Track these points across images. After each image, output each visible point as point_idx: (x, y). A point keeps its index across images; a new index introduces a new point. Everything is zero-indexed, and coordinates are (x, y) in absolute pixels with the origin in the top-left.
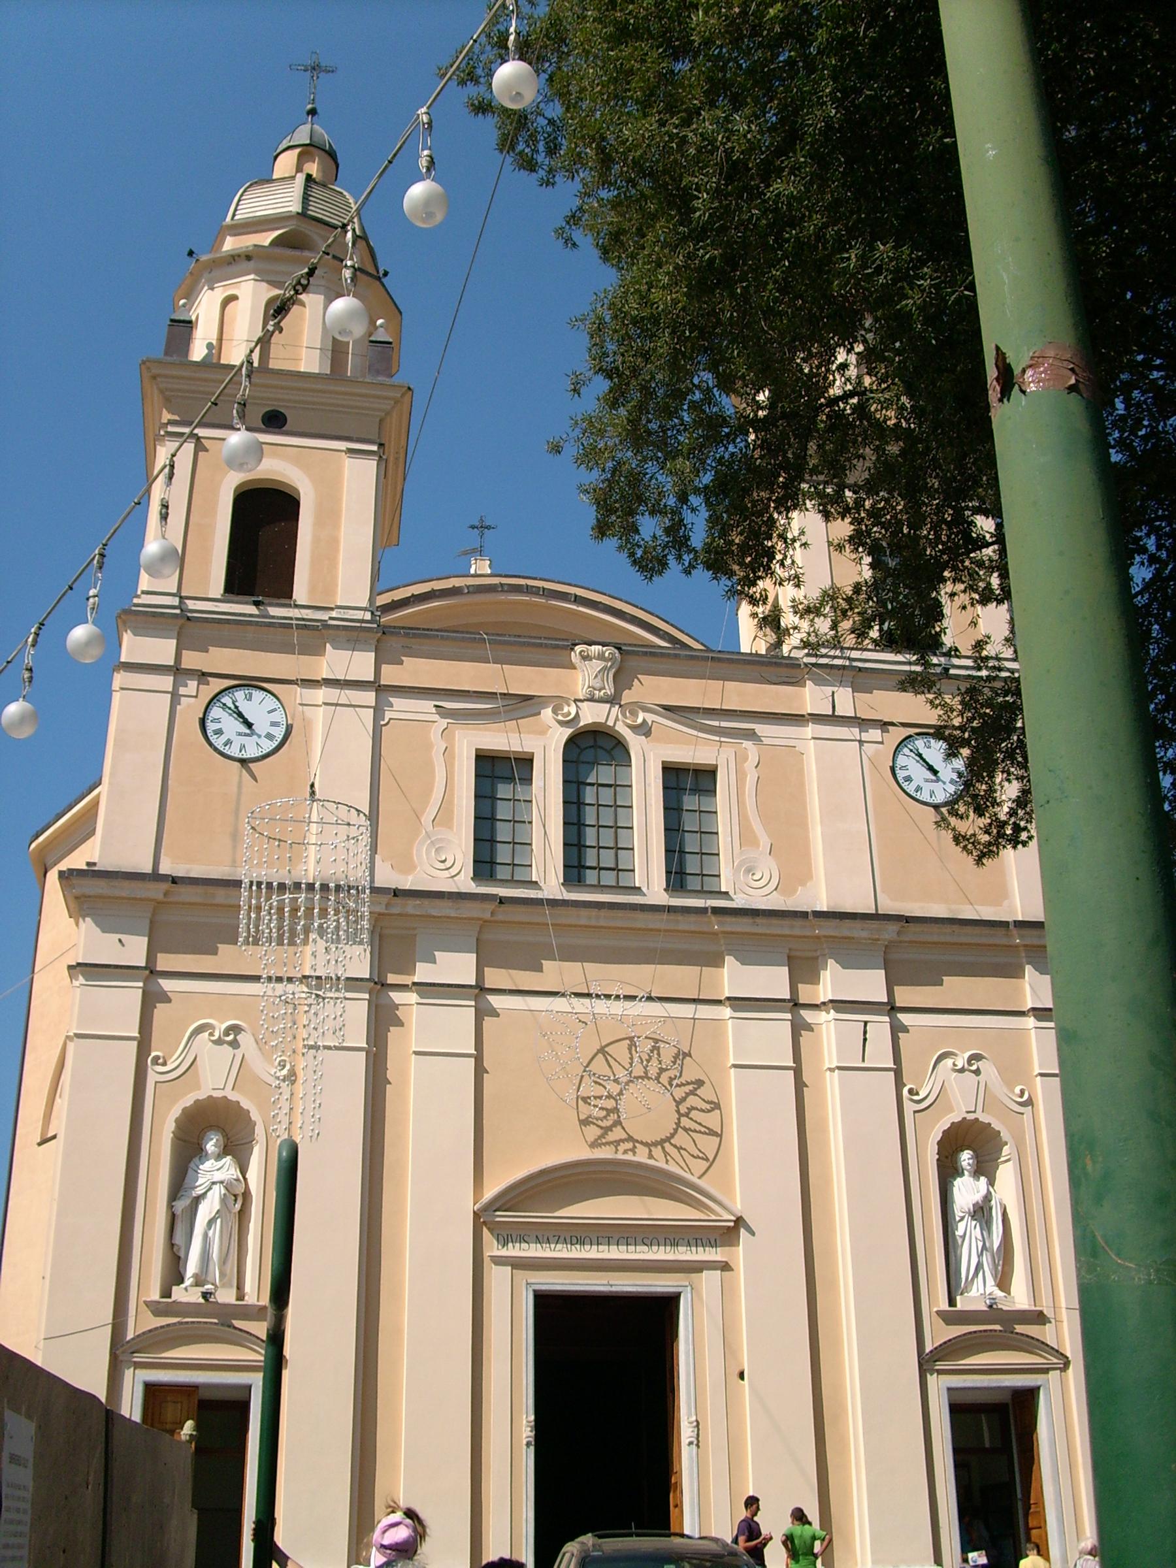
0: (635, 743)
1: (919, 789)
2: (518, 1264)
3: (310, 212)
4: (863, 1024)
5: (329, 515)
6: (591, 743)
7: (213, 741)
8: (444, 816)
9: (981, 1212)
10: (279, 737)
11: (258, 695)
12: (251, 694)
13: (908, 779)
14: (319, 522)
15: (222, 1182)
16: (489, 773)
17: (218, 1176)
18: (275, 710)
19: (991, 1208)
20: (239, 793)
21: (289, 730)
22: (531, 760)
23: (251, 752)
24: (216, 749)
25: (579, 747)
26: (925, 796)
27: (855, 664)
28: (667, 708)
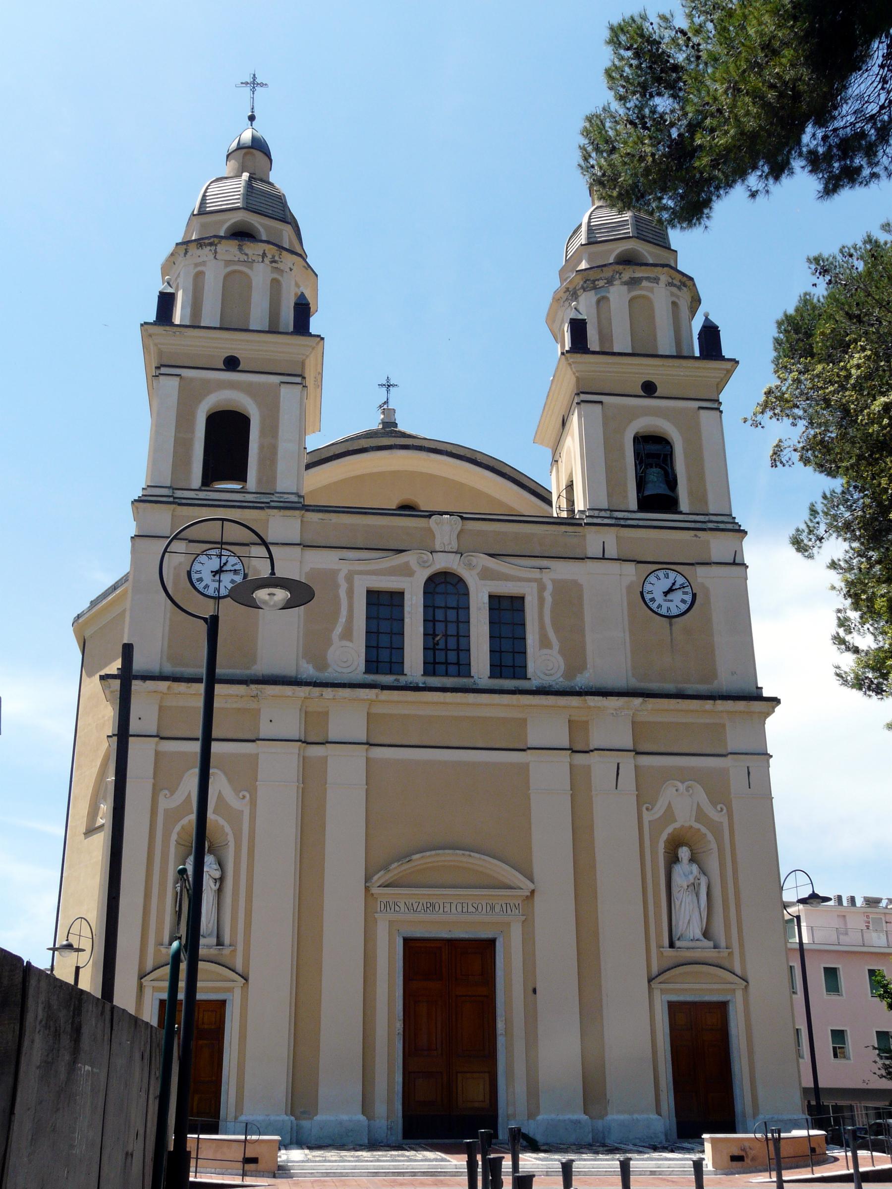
1: (659, 606)
3: (208, 209)
6: (443, 580)
7: (197, 586)
8: (347, 634)
14: (263, 433)
21: (694, 596)
23: (675, 611)
25: (435, 583)
26: (663, 611)
27: (177, 500)
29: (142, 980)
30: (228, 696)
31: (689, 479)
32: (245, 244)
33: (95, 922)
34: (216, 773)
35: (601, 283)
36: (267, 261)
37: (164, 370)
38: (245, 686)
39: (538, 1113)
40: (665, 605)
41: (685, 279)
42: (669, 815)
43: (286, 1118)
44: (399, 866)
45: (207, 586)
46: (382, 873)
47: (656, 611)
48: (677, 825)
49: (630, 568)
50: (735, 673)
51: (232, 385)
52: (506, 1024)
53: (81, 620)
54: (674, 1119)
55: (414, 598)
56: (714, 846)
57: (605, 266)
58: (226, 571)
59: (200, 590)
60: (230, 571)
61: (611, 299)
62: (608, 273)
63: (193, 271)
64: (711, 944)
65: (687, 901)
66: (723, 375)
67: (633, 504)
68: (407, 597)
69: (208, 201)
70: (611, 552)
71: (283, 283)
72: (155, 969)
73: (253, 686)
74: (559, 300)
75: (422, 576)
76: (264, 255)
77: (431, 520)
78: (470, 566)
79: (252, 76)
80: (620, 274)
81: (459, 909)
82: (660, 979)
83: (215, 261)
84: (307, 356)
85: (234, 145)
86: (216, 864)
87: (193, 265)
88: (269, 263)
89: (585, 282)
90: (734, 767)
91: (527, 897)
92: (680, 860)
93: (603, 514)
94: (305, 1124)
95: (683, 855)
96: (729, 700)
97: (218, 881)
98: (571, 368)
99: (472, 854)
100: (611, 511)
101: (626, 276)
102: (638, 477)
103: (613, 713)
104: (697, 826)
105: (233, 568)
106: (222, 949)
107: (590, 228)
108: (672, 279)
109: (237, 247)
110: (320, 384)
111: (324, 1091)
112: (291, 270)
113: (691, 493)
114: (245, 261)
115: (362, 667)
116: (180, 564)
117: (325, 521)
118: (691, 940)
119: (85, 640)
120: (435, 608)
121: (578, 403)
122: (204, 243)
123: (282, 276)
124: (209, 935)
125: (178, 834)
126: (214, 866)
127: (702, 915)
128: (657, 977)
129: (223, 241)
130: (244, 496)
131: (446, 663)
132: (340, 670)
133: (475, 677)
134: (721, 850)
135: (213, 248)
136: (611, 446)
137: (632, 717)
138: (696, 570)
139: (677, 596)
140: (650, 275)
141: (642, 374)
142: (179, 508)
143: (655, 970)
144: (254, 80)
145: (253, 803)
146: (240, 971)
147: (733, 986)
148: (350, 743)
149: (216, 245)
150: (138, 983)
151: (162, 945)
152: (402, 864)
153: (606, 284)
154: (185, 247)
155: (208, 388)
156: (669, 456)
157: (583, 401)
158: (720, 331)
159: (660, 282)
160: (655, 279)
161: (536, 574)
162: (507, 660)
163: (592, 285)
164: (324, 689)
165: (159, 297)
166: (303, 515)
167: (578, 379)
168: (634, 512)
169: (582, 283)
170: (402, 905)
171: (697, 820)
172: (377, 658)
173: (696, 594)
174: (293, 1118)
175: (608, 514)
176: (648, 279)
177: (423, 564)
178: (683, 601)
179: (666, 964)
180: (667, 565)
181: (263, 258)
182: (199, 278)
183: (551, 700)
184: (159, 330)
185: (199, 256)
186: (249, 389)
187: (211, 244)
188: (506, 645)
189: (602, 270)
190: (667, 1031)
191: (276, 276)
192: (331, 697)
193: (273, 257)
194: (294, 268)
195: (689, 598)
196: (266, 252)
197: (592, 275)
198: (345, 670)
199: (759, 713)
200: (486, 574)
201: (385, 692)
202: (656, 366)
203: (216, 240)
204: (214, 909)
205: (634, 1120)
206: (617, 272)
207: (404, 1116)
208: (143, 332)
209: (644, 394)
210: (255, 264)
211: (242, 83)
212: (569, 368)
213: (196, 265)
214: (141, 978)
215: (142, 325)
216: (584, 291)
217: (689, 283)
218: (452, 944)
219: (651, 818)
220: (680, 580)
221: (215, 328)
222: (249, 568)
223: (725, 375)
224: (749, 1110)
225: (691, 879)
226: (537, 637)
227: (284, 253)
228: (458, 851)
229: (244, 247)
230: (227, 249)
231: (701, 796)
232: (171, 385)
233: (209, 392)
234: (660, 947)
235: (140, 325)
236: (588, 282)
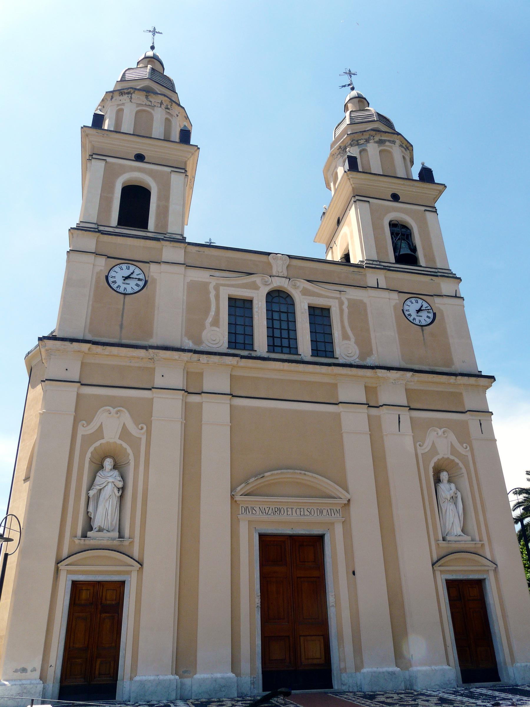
1: (414, 319)
7: (112, 286)
8: (216, 323)
9: (454, 499)
12: (129, 267)
14: (159, 199)
20: (123, 309)
21: (435, 314)
24: (113, 289)
26: (417, 322)
29: (58, 565)
30: (132, 357)
31: (424, 249)
32: (150, 95)
33: (23, 516)
34: (122, 410)
35: (362, 142)
36: (163, 107)
37: (94, 156)
38: (145, 350)
39: (362, 667)
40: (418, 319)
41: (409, 145)
42: (434, 450)
43: (172, 677)
44: (255, 480)
45: (119, 287)
46: (243, 485)
47: (413, 322)
48: (439, 457)
49: (395, 295)
50: (465, 361)
51: (140, 170)
52: (335, 598)
53: (30, 355)
54: (459, 668)
55: (260, 303)
56: (464, 470)
57: (365, 131)
58: (133, 278)
59: (114, 288)
60: (136, 278)
61: (369, 150)
62: (366, 136)
63: (115, 109)
64: (469, 538)
65: (450, 509)
66: (437, 194)
67: (393, 260)
68: (255, 302)
69: (126, 76)
70: (382, 284)
71: (173, 122)
72: (69, 557)
73: (150, 351)
74: (333, 155)
75: (265, 290)
76: (161, 103)
77: (270, 256)
78: (295, 287)
79: (153, 28)
80: (374, 137)
81: (298, 513)
82: (439, 563)
83: (130, 103)
84: (188, 159)
85: (143, 56)
86: (119, 477)
87: (116, 106)
88: (164, 108)
89: (352, 141)
90: (472, 420)
91: (345, 504)
92: (442, 481)
93: (374, 263)
94: (187, 681)
95: (444, 477)
96: (465, 376)
97: (120, 489)
98: (350, 181)
99: (306, 473)
100: (380, 262)
101: (377, 138)
102: (394, 244)
103: (393, 382)
104: (452, 457)
105: (138, 277)
106: (123, 540)
107: (351, 117)
108: (402, 143)
109: (145, 97)
110: (192, 186)
111: (201, 655)
112: (177, 116)
113: (425, 256)
114: (149, 105)
115: (226, 345)
116: (101, 270)
117: (200, 252)
118: (456, 536)
119: (32, 368)
120: (273, 311)
121: (355, 202)
122: (124, 92)
123: (172, 118)
124: (112, 531)
125: (91, 453)
126: (119, 478)
127: (460, 519)
128: (437, 561)
129: (136, 92)
130: (146, 234)
131: (282, 346)
132: (211, 345)
133: (302, 355)
134: (469, 473)
135: (130, 95)
136: (376, 227)
137: (405, 385)
138: (434, 299)
139: (424, 314)
140: (390, 139)
141: (392, 188)
142: (102, 236)
143: (435, 559)
144: (155, 30)
145: (149, 433)
146: (137, 559)
147: (486, 568)
148: (219, 394)
149: (131, 94)
150: (55, 567)
151: (76, 537)
152: (257, 479)
153: (365, 142)
154: (111, 94)
155: (124, 170)
156: (409, 236)
157: (357, 200)
158: (432, 171)
159: (396, 144)
160: (393, 142)
161: (337, 294)
162: (321, 347)
163: (356, 143)
164: (201, 356)
165: (94, 115)
166: (186, 247)
167: (353, 189)
168: (393, 263)
169: (350, 142)
170: (257, 509)
171: (452, 454)
172: (235, 340)
173: (435, 313)
174: (177, 677)
175: (378, 263)
176: (389, 141)
177: (266, 284)
178: (428, 317)
179: (442, 553)
180: (417, 295)
181: (161, 105)
182: (119, 113)
183: (354, 371)
184: (94, 131)
185: (120, 100)
186: (150, 173)
187: (128, 93)
188: (320, 338)
189: (363, 134)
190: (447, 601)
191: (168, 116)
192: (205, 362)
193: (167, 105)
194: (179, 115)
195: (431, 315)
196: (163, 101)
197: (356, 137)
198: (214, 346)
199: (482, 386)
200: (305, 292)
201: (243, 360)
202: (399, 184)
203: (132, 91)
204: (117, 510)
205: (433, 670)
206: (372, 136)
207: (264, 673)
208: (82, 132)
209: (392, 200)
210: (155, 108)
211: (147, 30)
212: (348, 181)
213: (118, 105)
214: (58, 563)
215: (82, 128)
216: (352, 146)
217: (410, 148)
218: (293, 538)
219: (423, 452)
220: (425, 305)
221: (130, 134)
222: (148, 277)
223: (438, 194)
224: (508, 659)
225: (452, 492)
226: (340, 332)
227: (174, 104)
228: (297, 471)
229: (149, 97)
230: (139, 97)
231: (452, 437)
232: (99, 166)
233: (124, 173)
234: (437, 541)
235: (68, 230)
236: (354, 141)
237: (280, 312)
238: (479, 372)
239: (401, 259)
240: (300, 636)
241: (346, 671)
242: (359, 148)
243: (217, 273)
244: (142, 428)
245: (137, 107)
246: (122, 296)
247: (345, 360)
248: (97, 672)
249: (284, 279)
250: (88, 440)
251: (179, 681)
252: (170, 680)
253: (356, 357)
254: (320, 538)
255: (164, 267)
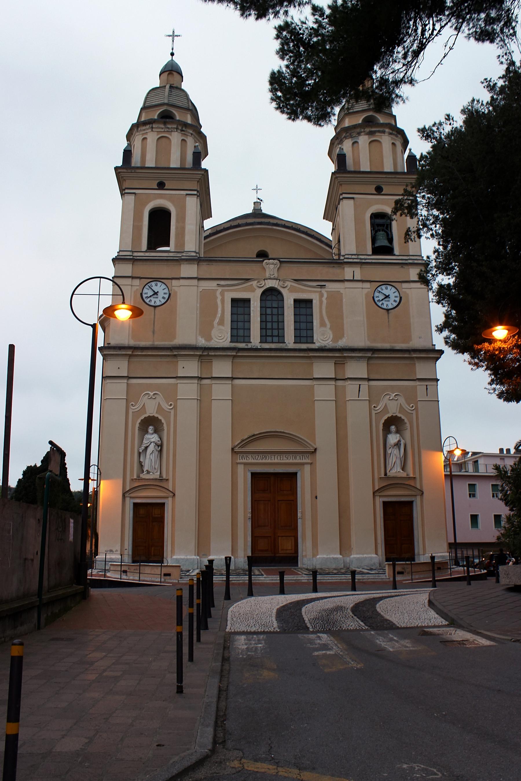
0: (284, 292)
2: (245, 464)
4: (426, 386)
5: (182, 218)
8: (221, 322)
9: (398, 445)
10: (398, 301)
11: (159, 284)
12: (157, 284)
13: (164, 298)
14: (177, 221)
15: (154, 442)
16: (264, 306)
17: (153, 440)
18: (165, 289)
19: (400, 444)
22: (250, 301)
28: (295, 280)
61: (360, 143)
90: (421, 387)
93: (353, 257)
100: (358, 255)
116: (137, 289)
132: (218, 341)
174: (198, 557)
186: (170, 198)
200: (292, 290)
237: (272, 308)
238: (433, 345)
239: (376, 251)
240: (279, 536)
241: (306, 557)
242: (352, 140)
243: (222, 283)
244: (171, 405)
245: (157, 135)
246: (153, 308)
247: (320, 344)
248: (152, 554)
249: (275, 281)
250: (136, 414)
251: (199, 560)
252: (194, 559)
253: (330, 340)
254: (294, 475)
255: (182, 282)
